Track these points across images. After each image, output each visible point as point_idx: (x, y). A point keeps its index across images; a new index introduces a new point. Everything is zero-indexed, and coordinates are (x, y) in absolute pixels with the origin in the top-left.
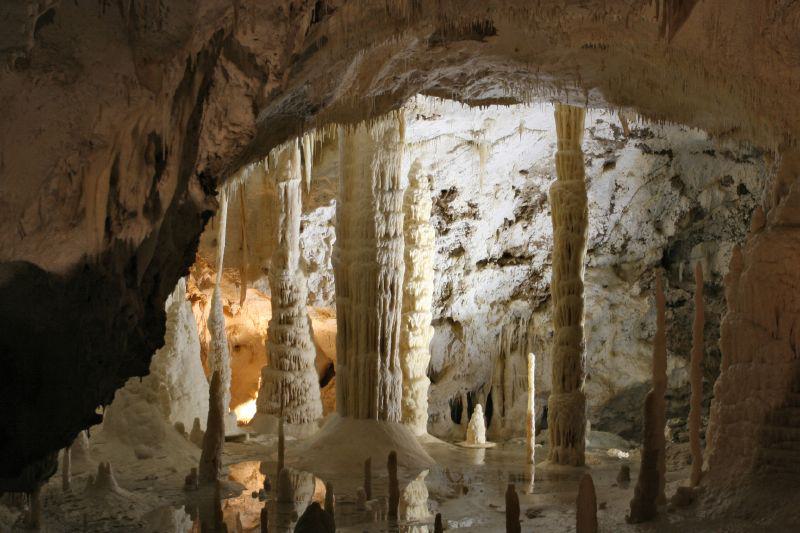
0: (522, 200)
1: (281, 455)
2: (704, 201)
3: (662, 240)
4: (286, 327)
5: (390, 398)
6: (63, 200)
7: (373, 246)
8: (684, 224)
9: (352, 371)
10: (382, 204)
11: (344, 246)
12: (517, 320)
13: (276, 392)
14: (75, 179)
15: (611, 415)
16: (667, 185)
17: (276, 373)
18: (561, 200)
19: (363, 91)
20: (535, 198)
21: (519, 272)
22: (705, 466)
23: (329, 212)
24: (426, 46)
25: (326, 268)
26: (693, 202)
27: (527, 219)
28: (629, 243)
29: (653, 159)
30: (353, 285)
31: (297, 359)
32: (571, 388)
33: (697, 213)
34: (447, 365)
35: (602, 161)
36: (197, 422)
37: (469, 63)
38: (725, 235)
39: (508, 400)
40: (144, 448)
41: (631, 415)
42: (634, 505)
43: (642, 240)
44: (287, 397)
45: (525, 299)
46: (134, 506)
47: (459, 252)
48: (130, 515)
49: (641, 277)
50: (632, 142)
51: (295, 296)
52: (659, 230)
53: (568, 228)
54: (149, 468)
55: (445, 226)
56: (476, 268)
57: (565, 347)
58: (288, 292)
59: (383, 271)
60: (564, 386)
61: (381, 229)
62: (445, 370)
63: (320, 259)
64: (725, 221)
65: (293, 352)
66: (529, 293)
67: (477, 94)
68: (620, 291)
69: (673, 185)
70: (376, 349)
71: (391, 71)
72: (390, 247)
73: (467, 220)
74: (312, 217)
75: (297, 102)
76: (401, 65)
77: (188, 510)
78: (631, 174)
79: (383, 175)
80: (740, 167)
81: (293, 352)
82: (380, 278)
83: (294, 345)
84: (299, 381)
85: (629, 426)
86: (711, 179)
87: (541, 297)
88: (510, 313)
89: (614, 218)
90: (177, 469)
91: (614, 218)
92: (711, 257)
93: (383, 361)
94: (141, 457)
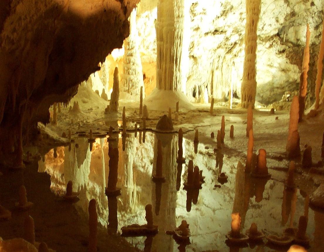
0: (223, 8)
2: (296, 9)
3: (278, 26)
4: (131, 57)
5: (179, 82)
7: (174, 20)
8: (288, 18)
9: (164, 71)
10: (177, 3)
11: (161, 21)
12: (219, 57)
13: (127, 83)
17: (127, 75)
18: (251, 2)
20: (229, 7)
21: (220, 38)
22: (320, 103)
26: (292, 9)
27: (225, 16)
28: (265, 26)
30: (164, 36)
31: (135, 70)
32: (251, 79)
34: (190, 75)
40: (86, 100)
43: (270, 25)
44: (131, 85)
45: (223, 48)
46: (89, 118)
47: (197, 29)
48: (88, 121)
51: (134, 45)
52: (277, 21)
53: (253, 14)
56: (204, 35)
57: (250, 62)
58: (131, 44)
59: (177, 31)
60: (248, 78)
61: (176, 13)
64: (304, 18)
65: (133, 67)
66: (224, 46)
70: (173, 62)
72: (180, 21)
73: (201, 15)
81: (133, 67)
82: (176, 33)
83: (134, 64)
84: (136, 79)
87: (229, 48)
90: (99, 107)
92: (296, 32)
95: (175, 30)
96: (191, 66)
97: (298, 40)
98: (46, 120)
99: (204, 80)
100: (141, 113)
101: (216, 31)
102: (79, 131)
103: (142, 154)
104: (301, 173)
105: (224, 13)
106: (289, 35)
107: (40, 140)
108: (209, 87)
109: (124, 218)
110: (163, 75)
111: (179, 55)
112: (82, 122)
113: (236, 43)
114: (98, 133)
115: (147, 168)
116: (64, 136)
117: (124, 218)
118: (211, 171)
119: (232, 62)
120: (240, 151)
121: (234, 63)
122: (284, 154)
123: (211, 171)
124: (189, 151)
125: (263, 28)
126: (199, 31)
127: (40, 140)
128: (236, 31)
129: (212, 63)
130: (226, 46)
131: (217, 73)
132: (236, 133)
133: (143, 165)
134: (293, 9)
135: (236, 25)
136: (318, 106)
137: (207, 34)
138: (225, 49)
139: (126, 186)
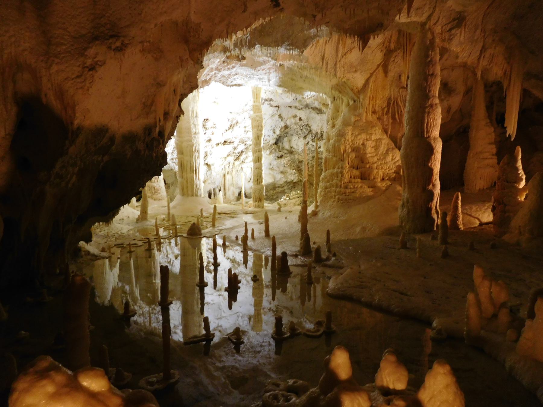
2: (288, 123)
3: (275, 136)
7: (191, 137)
8: (282, 130)
9: (185, 181)
12: (229, 163)
20: (234, 122)
22: (318, 204)
29: (273, 109)
33: (286, 127)
37: (235, 69)
47: (210, 140)
49: (269, 148)
52: (274, 133)
61: (193, 131)
71: (208, 71)
76: (212, 70)
79: (193, 111)
80: (299, 111)
82: (194, 148)
86: (290, 116)
88: (227, 161)
93: (196, 176)
95: (193, 145)
97: (291, 147)
98: (88, 240)
99: (217, 184)
100: (169, 220)
101: (225, 142)
102: (116, 243)
103: (167, 251)
104: (315, 268)
105: (231, 127)
106: (284, 144)
108: (222, 189)
109: (154, 311)
110: (185, 183)
111: (197, 166)
112: (117, 233)
113: (242, 152)
114: (135, 244)
115: (173, 263)
117: (154, 311)
118: (229, 260)
119: (240, 168)
120: (262, 251)
121: (242, 168)
123: (229, 260)
124: (208, 244)
126: (211, 142)
127: (82, 257)
128: (242, 142)
131: (228, 177)
132: (256, 234)
133: (169, 260)
134: (285, 123)
135: (242, 137)
136: (317, 207)
137: (218, 144)
138: (233, 157)
139: (154, 281)
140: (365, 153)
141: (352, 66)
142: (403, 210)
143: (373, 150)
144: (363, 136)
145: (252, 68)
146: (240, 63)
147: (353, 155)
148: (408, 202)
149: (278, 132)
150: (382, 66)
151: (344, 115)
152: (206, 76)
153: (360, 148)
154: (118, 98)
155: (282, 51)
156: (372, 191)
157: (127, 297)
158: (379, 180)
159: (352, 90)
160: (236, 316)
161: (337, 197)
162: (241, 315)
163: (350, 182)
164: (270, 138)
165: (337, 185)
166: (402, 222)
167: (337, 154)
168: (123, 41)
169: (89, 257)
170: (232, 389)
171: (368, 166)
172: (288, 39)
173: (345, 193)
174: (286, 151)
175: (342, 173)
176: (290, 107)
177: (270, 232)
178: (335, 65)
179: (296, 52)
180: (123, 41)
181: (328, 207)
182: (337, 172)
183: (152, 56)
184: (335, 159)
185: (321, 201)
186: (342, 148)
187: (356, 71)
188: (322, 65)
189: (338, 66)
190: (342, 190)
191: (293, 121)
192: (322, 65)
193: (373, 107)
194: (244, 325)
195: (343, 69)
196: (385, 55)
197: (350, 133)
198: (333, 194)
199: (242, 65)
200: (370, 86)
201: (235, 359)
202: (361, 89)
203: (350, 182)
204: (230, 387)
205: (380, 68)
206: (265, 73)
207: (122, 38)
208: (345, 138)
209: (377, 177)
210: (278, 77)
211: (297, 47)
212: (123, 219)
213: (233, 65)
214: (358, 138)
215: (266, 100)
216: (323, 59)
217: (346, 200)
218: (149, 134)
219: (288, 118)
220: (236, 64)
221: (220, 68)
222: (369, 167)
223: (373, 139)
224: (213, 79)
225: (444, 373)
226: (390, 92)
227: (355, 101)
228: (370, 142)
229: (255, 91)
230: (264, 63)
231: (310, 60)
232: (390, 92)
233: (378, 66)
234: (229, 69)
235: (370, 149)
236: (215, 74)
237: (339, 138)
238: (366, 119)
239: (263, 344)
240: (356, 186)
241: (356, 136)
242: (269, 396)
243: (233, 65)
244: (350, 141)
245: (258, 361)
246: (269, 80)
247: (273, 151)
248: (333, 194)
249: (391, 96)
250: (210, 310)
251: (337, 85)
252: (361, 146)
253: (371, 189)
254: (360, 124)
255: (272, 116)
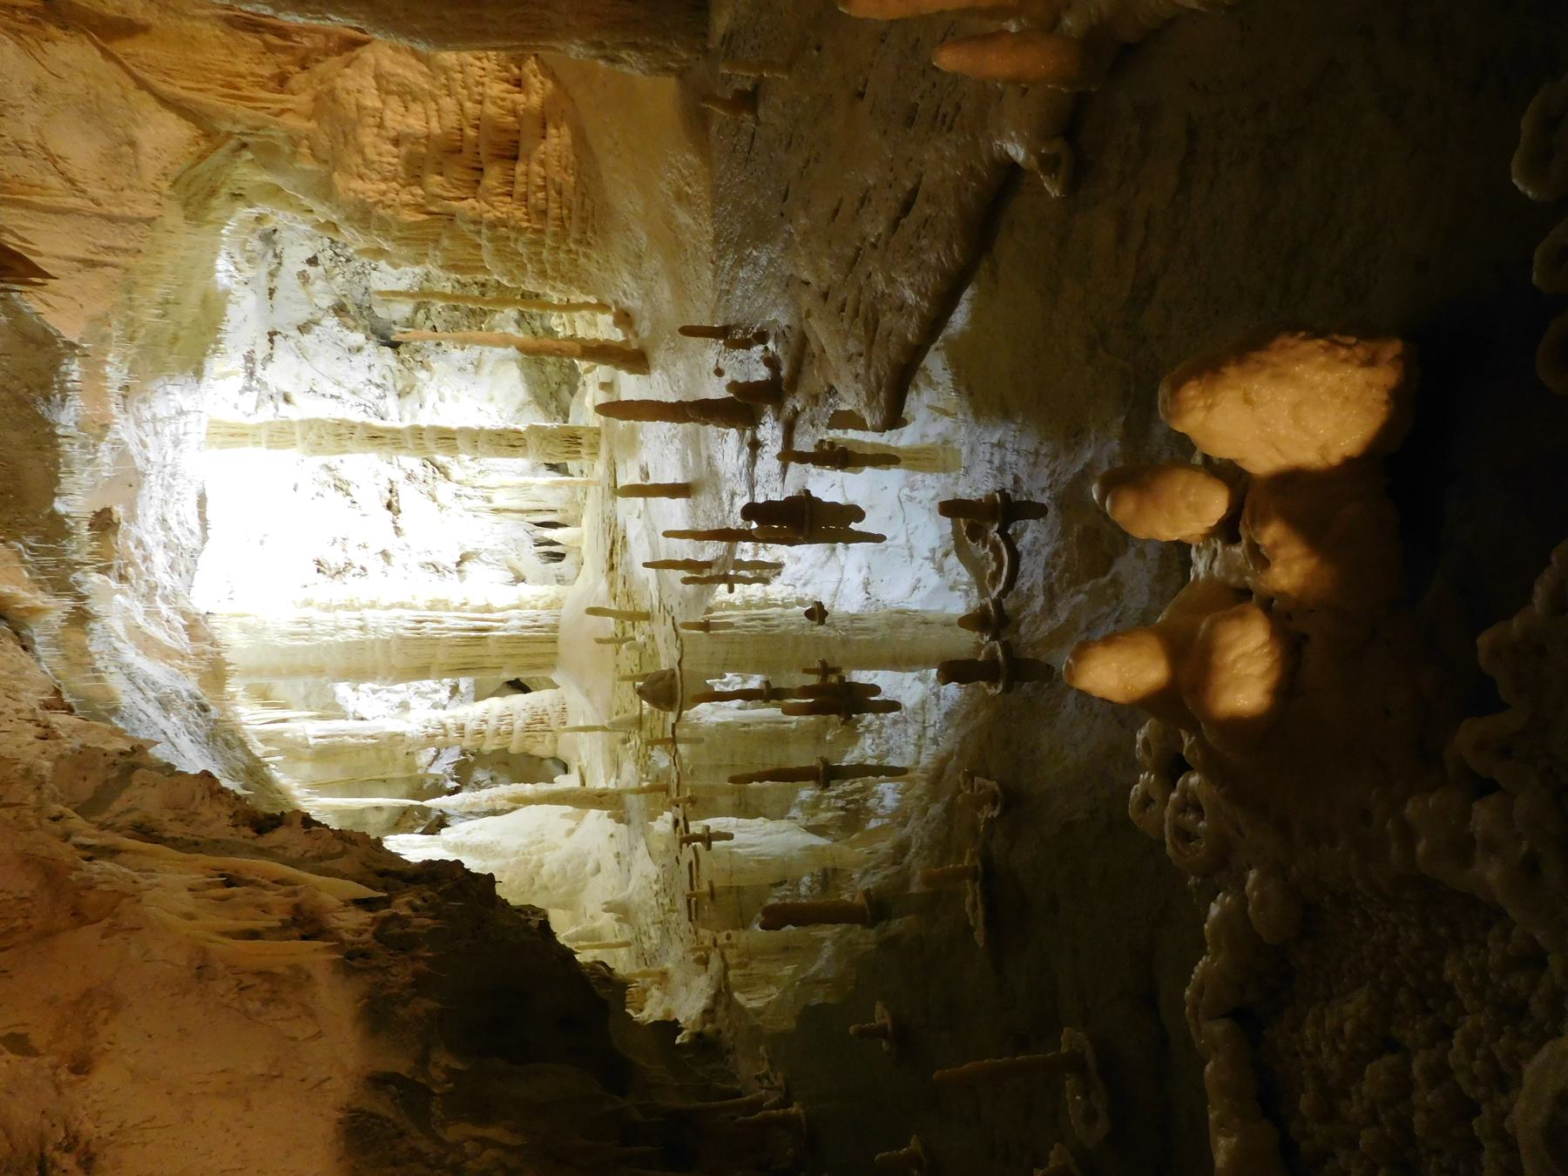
1: (594, 729)
2: (327, 301)
3: (370, 347)
4: (467, 730)
6: (275, 992)
7: (373, 642)
8: (351, 323)
9: (509, 660)
14: (248, 981)
15: (554, 405)
16: (307, 339)
19: (182, 657)
20: (325, 476)
21: (409, 497)
22: (594, 301)
23: (343, 690)
24: (125, 586)
25: (404, 690)
31: (501, 718)
35: (282, 405)
36: (564, 816)
37: (147, 539)
38: (364, 282)
39: (541, 506)
40: (590, 866)
41: (554, 386)
42: (632, 371)
47: (385, 554)
49: (410, 369)
50: (259, 372)
52: (359, 350)
54: (609, 863)
55: (358, 570)
58: (430, 730)
59: (401, 631)
61: (354, 635)
62: (512, 569)
63: (396, 699)
67: (192, 533)
68: (426, 391)
69: (308, 332)
71: (158, 625)
74: (350, 709)
75: (193, 728)
76: (152, 614)
77: (654, 819)
78: (298, 376)
80: (286, 262)
81: (493, 722)
82: (408, 634)
83: (486, 722)
85: (565, 387)
86: (302, 294)
89: (346, 395)
91: (346, 395)
93: (497, 629)
94: (598, 870)
95: (400, 637)
96: (483, 566)
99: (521, 534)
101: (389, 506)
106: (395, 317)
107: (719, 1032)
114: (690, 865)
116: (704, 962)
117: (874, 727)
122: (742, 436)
125: (378, 386)
127: (719, 1032)
129: (475, 513)
130: (430, 480)
131: (500, 500)
137: (397, 530)
140: (428, 137)
141: (112, 158)
142: (625, 62)
143: (416, 107)
144: (367, 136)
145: (140, 485)
146: (124, 524)
147: (434, 182)
148: (600, 45)
149: (358, 338)
150: (108, 40)
151: (295, 188)
152: (175, 629)
153: (411, 153)
154: (248, 1106)
155: (67, 418)
156: (557, 128)
157: (830, 798)
158: (520, 97)
159: (201, 157)
160: (907, 505)
161: (573, 247)
162: (906, 491)
163: (525, 198)
164: (378, 363)
165: (533, 243)
166: (667, 69)
167: (430, 232)
168: (58, 1147)
169: (720, 1012)
170: (1109, 577)
171: (471, 133)
172: (22, 403)
173: (562, 219)
174: (421, 315)
175: (492, 225)
176: (272, 292)
177: (680, 481)
178: (112, 219)
179: (74, 370)
180: (58, 1147)
181: (606, 275)
182: (490, 240)
183: (106, 1022)
184: (446, 242)
185: (582, 289)
186: (409, 216)
187: (132, 144)
188: (115, 266)
189: (116, 211)
190: (551, 227)
191: (319, 285)
192: (115, 266)
193: (263, 87)
194: (938, 486)
195: (127, 192)
196: (65, 28)
197: (357, 184)
198: (562, 255)
199: (132, 518)
200: (184, 93)
201: (1029, 553)
202: (199, 127)
203: (525, 198)
204: (1104, 580)
205: (121, 47)
206: (156, 433)
207: (50, 1147)
208: (376, 203)
209: (508, 104)
210: (169, 388)
211: (54, 367)
212: (618, 855)
213: (131, 545)
214: (376, 158)
215: (251, 374)
216: (92, 264)
217: (584, 220)
218: (364, 955)
219: (310, 302)
220: (127, 536)
221: (143, 588)
222: (477, 127)
223: (378, 104)
224: (182, 603)
225: (1209, 408)
226: (206, 18)
227: (244, 146)
228: (388, 115)
229: (219, 439)
230: (123, 454)
231: (96, 308)
232: (206, 18)
233: (108, 55)
234: (145, 559)
235: (411, 121)
236: (165, 599)
237: (374, 221)
238: (309, 119)
239: (997, 462)
240: (540, 182)
241: (367, 163)
242: (1175, 846)
243: (131, 545)
244: (383, 186)
245: (1043, 490)
246: (181, 413)
247: (419, 359)
248: (562, 255)
249: (220, 17)
250: (886, 579)
251: (186, 205)
252: (403, 150)
253: (552, 131)
254: (324, 141)
255: (302, 353)
